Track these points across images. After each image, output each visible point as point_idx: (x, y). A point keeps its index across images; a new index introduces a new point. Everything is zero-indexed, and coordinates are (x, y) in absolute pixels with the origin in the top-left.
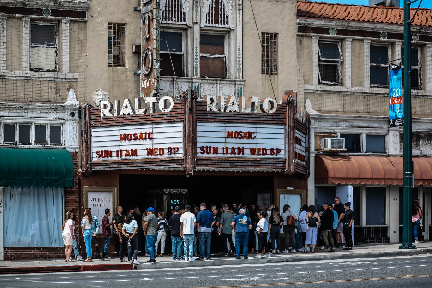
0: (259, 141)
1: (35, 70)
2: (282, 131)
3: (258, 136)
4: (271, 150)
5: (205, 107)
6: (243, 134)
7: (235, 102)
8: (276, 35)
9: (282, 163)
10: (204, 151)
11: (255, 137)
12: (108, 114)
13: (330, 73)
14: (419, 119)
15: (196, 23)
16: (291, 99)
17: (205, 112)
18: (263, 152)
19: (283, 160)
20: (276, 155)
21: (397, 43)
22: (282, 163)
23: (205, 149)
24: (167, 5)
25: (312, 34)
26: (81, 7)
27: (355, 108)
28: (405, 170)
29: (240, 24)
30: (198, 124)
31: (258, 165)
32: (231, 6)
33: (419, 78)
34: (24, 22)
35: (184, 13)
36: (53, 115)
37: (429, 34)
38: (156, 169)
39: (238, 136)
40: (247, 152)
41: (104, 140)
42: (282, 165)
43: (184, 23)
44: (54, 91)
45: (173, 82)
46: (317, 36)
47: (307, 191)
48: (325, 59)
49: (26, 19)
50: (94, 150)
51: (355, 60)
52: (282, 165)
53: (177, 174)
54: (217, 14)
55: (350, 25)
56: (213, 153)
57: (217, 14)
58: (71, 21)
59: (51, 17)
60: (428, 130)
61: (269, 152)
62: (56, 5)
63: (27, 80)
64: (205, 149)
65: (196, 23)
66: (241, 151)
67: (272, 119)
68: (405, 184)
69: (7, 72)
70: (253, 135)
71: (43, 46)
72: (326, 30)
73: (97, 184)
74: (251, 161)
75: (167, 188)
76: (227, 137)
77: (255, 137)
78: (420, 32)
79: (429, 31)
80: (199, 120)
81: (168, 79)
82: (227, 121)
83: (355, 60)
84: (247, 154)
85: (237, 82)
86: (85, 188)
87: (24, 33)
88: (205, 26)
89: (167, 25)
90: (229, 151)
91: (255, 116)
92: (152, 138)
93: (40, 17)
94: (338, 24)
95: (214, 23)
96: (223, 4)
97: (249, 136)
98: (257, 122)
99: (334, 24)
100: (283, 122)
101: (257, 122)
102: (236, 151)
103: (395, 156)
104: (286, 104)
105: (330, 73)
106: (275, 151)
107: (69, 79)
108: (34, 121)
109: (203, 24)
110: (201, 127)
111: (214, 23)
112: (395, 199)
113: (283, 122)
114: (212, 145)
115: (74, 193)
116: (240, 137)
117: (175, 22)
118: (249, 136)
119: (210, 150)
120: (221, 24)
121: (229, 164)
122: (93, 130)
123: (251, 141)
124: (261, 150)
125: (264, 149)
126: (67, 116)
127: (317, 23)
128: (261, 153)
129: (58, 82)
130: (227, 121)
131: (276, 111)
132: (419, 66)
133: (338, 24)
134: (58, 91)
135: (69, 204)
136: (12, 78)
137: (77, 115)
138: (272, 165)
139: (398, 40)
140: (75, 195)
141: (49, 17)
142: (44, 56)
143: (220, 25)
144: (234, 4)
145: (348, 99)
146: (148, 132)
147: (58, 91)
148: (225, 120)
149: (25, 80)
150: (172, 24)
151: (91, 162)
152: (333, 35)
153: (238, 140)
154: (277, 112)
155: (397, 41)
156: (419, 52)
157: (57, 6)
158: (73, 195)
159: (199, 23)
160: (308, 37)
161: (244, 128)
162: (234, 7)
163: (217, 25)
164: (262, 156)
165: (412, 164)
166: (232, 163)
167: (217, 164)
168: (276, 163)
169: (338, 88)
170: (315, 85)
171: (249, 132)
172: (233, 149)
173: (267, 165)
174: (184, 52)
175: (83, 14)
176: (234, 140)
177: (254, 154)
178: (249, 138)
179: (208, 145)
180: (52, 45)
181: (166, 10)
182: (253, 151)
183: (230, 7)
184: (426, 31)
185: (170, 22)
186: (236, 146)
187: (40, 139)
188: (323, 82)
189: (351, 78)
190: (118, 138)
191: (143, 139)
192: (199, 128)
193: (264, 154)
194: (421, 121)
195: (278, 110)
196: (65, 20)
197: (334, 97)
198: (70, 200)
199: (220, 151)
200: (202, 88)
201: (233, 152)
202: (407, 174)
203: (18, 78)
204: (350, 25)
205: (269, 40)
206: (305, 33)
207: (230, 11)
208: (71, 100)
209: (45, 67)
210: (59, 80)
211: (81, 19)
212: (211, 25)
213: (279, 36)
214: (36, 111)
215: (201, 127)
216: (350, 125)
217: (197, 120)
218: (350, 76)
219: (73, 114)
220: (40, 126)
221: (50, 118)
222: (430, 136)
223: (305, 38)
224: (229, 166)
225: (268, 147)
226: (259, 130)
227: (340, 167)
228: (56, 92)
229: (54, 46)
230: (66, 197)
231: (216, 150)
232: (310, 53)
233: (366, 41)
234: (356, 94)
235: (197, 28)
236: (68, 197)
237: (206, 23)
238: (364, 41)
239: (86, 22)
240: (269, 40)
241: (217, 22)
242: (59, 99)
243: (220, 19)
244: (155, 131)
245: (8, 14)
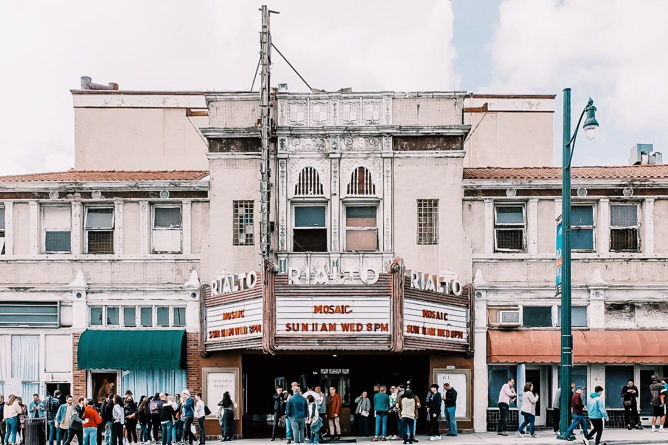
0: (356, 316)
1: (159, 253)
2: (388, 303)
3: (354, 310)
4: (367, 325)
5: (409, 282)
6: (334, 309)
7: (324, 273)
8: (436, 203)
9: (387, 339)
10: (290, 328)
11: (351, 311)
12: (417, 287)
13: (510, 238)
14: (632, 287)
15: (335, 194)
16: (395, 267)
17: (285, 285)
18: (358, 328)
19: (387, 336)
20: (375, 331)
21: (601, 200)
22: (387, 339)
23: (291, 326)
24: (301, 178)
25: (482, 197)
26: (200, 187)
27: (544, 277)
28: (563, 345)
29: (388, 193)
30: (278, 299)
31: (355, 342)
32: (378, 174)
33: (638, 239)
34: (141, 205)
35: (322, 186)
36: (175, 296)
37: (648, 186)
38: (256, 348)
39: (328, 310)
40: (339, 328)
41: (215, 320)
42: (386, 342)
43: (320, 195)
44: (175, 272)
45: (307, 257)
46: (490, 199)
47: (473, 371)
48: (501, 224)
49: (144, 202)
50: (208, 331)
51: (542, 222)
52: (386, 342)
53: (311, 353)
54: (361, 182)
55: (532, 183)
56: (302, 330)
57: (361, 182)
58: (193, 202)
59: (170, 199)
60: (647, 298)
61: (365, 327)
62: (172, 186)
63: (146, 262)
64: (291, 326)
65: (335, 194)
66: (333, 327)
67: (373, 291)
68: (563, 361)
69: (124, 255)
70: (348, 310)
71: (168, 228)
72: (503, 192)
73: (217, 365)
74: (345, 338)
75: (324, 368)
76: (315, 313)
77: (351, 311)
78: (634, 185)
79: (646, 183)
80: (278, 294)
81: (301, 255)
82: (314, 294)
83: (542, 222)
84: (339, 331)
85: (384, 255)
86: (205, 370)
87: (141, 216)
88: (346, 197)
89: (302, 199)
90: (319, 327)
91: (350, 288)
92: (446, 320)
93: (158, 199)
94: (515, 183)
95: (357, 193)
96: (369, 173)
97: (343, 310)
98: (353, 294)
99: (511, 184)
100: (388, 294)
101: (353, 294)
102: (328, 327)
103: (596, 330)
104: (391, 273)
105: (510, 238)
106: (373, 327)
107: (192, 260)
108: (154, 303)
109: (344, 194)
110: (280, 301)
111: (357, 193)
112: (599, 379)
113: (388, 294)
114: (301, 322)
115: (195, 374)
116: (331, 311)
117: (311, 195)
118: (343, 310)
119: (298, 327)
120: (367, 193)
121: (317, 342)
122: (209, 310)
123: (345, 315)
124: (355, 326)
125: (358, 325)
126: (188, 297)
127: (487, 184)
128: (355, 329)
129: (180, 265)
130: (314, 294)
131: (378, 281)
132: (639, 225)
133: (515, 183)
134: (179, 272)
135: (196, 385)
136: (129, 261)
137: (198, 296)
138: (374, 342)
139: (603, 196)
140: (196, 376)
141: (168, 199)
142: (166, 238)
143: (365, 195)
144: (381, 171)
145: (533, 267)
146: (444, 313)
147: (179, 272)
148: (311, 294)
149: (144, 263)
150: (352, 197)
151: (206, 343)
152: (511, 195)
153: (329, 316)
154: (379, 282)
155: (601, 198)
156: (638, 208)
157: (173, 187)
158: (194, 377)
159: (338, 195)
160: (480, 200)
161: (337, 302)
162: (382, 175)
163: (361, 195)
164: (356, 333)
165: (571, 339)
166: (321, 341)
167: (301, 342)
168: (378, 339)
169: (521, 256)
170: (488, 253)
171: (342, 306)
172: (324, 325)
173: (366, 342)
174: (327, 226)
175: (204, 194)
176: (324, 315)
177: (347, 331)
178: (343, 313)
179: (296, 322)
180: (178, 227)
181: (300, 183)
182: (345, 327)
183: (378, 175)
184: (642, 183)
185: (305, 195)
186: (327, 322)
187: (163, 319)
188: (499, 249)
189: (536, 243)
190: (222, 317)
191: (439, 319)
192: (278, 304)
193: (358, 330)
194: (635, 288)
195: (381, 280)
196: (185, 200)
197: (515, 265)
198: (191, 381)
199: (310, 328)
200: (342, 263)
201: (324, 328)
202: (565, 350)
203: (136, 261)
204: (532, 183)
205: (427, 209)
206: (474, 196)
207: (378, 179)
208: (194, 282)
209: (169, 250)
210: (180, 261)
211: (202, 198)
212: (354, 195)
213: (440, 202)
214: (157, 293)
215: (280, 301)
216: (537, 296)
217: (276, 294)
218: (536, 242)
219: (194, 295)
220: (114, 308)
221: (171, 300)
222: (650, 305)
223: (475, 202)
224: (318, 344)
225: (364, 322)
226: (356, 304)
227: (510, 343)
228: (178, 274)
229: (179, 228)
230: (188, 379)
231: (305, 327)
232: (482, 218)
233: (558, 200)
234: (544, 261)
235: (335, 201)
236: (189, 379)
237: (348, 193)
238: (555, 200)
239: (209, 201)
240: (427, 209)
241: (361, 192)
242: (180, 281)
243: (365, 189)
244: (246, 308)
245: (123, 199)
